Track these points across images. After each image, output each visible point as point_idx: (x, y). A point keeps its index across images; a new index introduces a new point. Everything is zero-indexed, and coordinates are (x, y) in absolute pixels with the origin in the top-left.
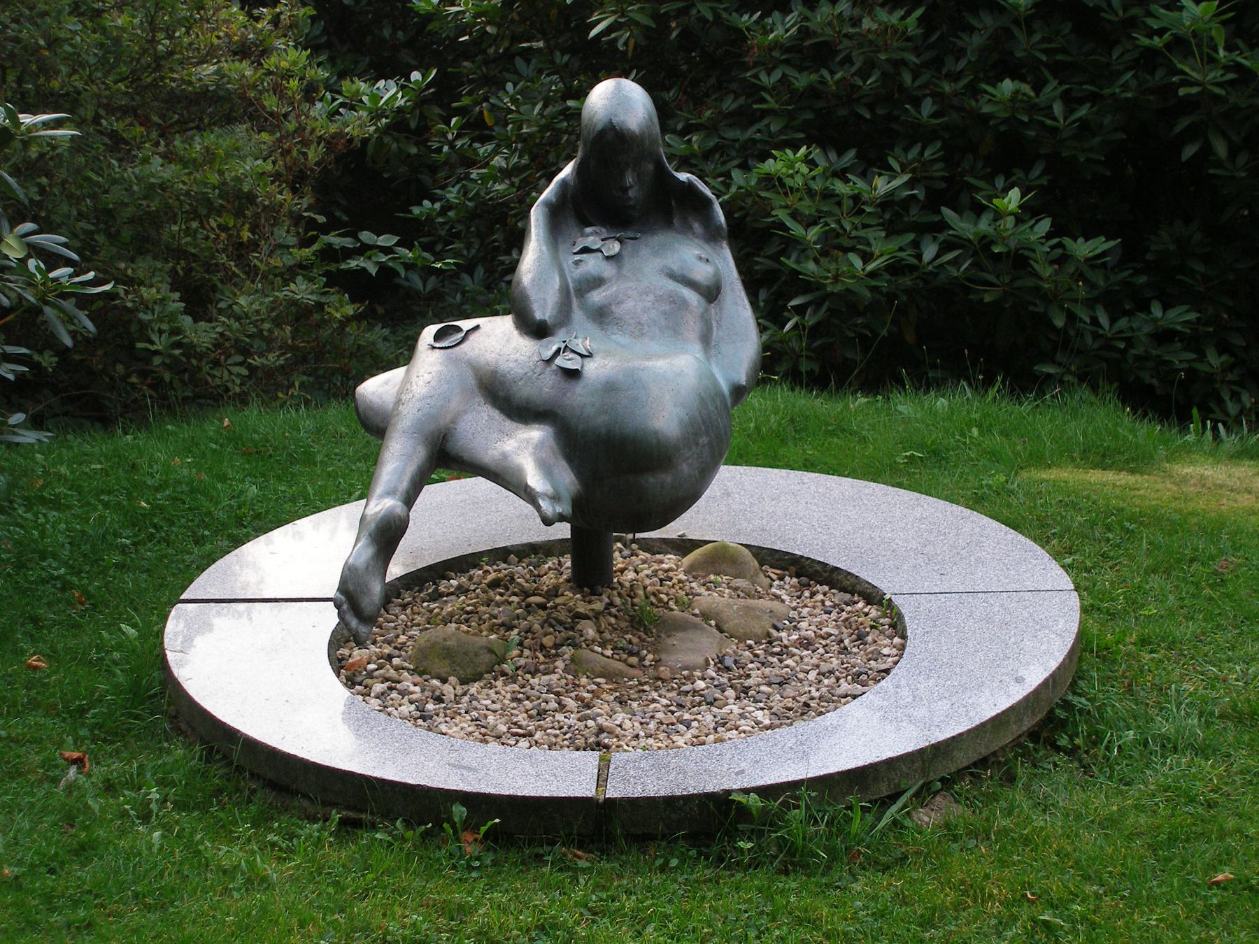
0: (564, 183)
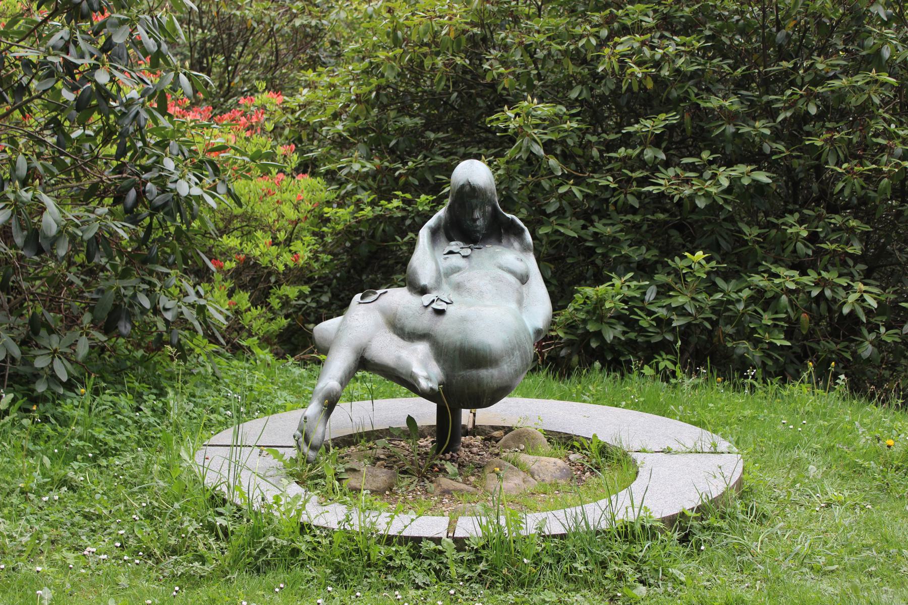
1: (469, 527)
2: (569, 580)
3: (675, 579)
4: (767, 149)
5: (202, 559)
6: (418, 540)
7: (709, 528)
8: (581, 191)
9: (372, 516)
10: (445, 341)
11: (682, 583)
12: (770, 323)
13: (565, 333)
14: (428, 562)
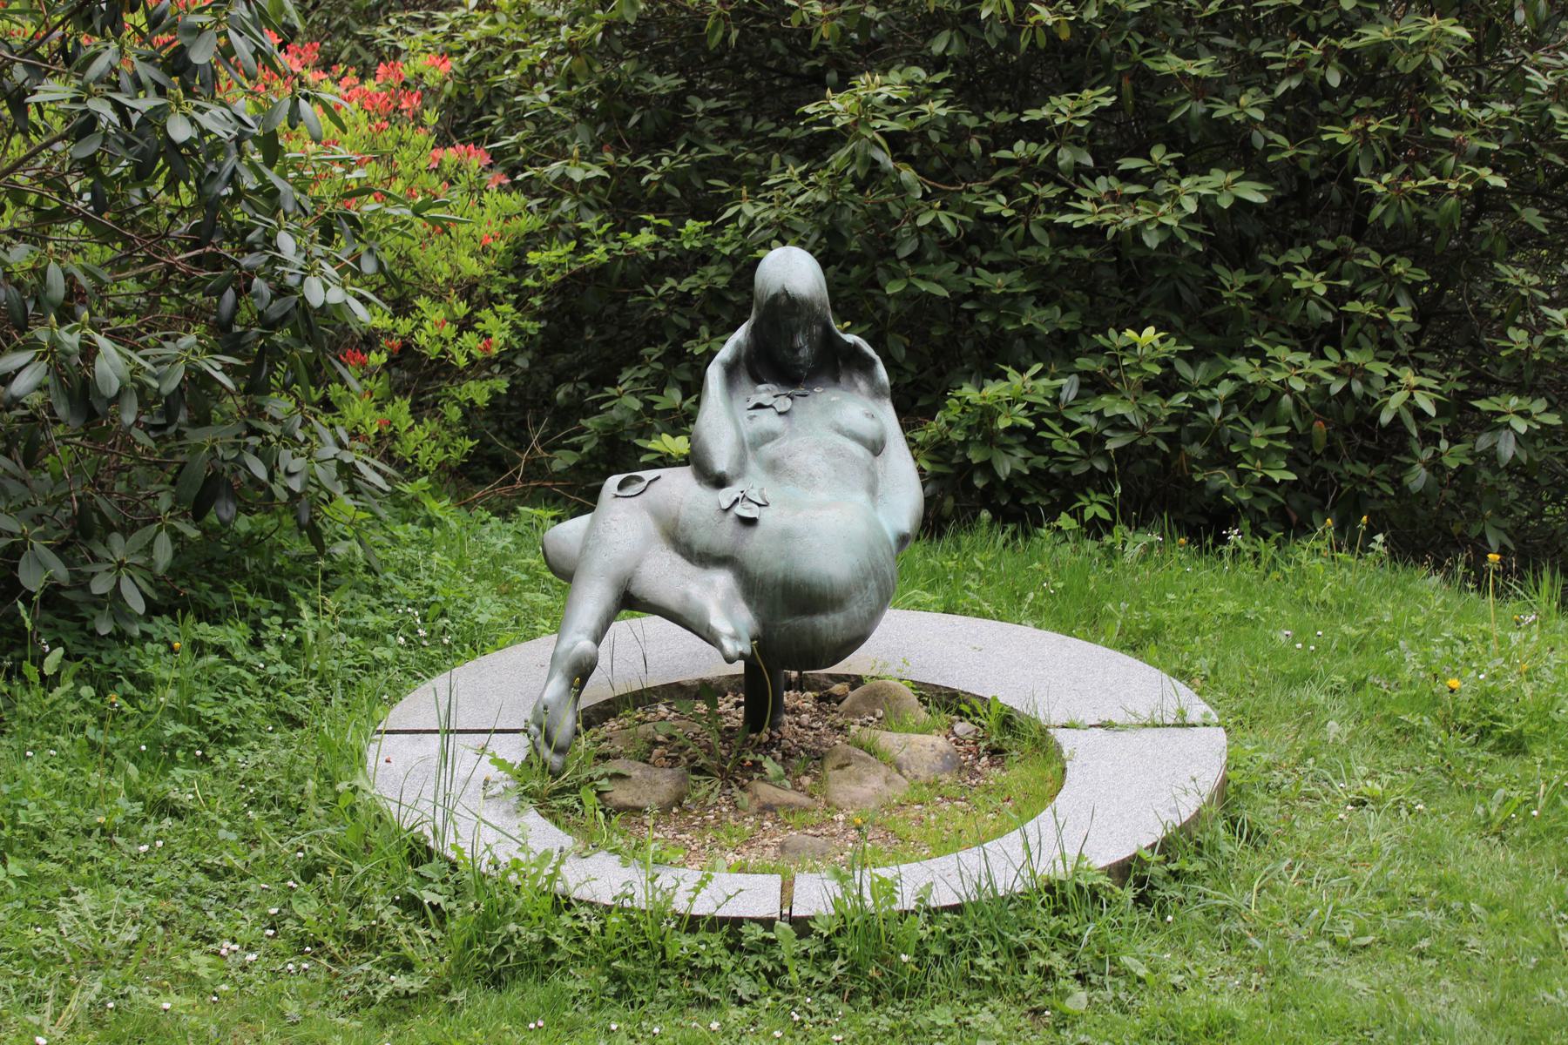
0: (738, 345)
1: (815, 896)
2: (969, 981)
3: (1127, 974)
4: (1258, 141)
5: (408, 967)
6: (738, 922)
7: (1176, 875)
8: (953, 219)
9: (666, 879)
10: (759, 571)
11: (1140, 980)
12: (1262, 444)
13: (932, 462)
14: (754, 958)
